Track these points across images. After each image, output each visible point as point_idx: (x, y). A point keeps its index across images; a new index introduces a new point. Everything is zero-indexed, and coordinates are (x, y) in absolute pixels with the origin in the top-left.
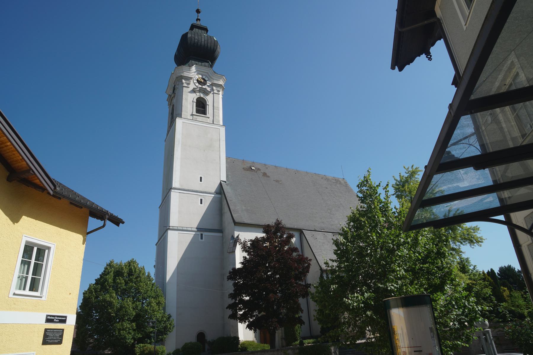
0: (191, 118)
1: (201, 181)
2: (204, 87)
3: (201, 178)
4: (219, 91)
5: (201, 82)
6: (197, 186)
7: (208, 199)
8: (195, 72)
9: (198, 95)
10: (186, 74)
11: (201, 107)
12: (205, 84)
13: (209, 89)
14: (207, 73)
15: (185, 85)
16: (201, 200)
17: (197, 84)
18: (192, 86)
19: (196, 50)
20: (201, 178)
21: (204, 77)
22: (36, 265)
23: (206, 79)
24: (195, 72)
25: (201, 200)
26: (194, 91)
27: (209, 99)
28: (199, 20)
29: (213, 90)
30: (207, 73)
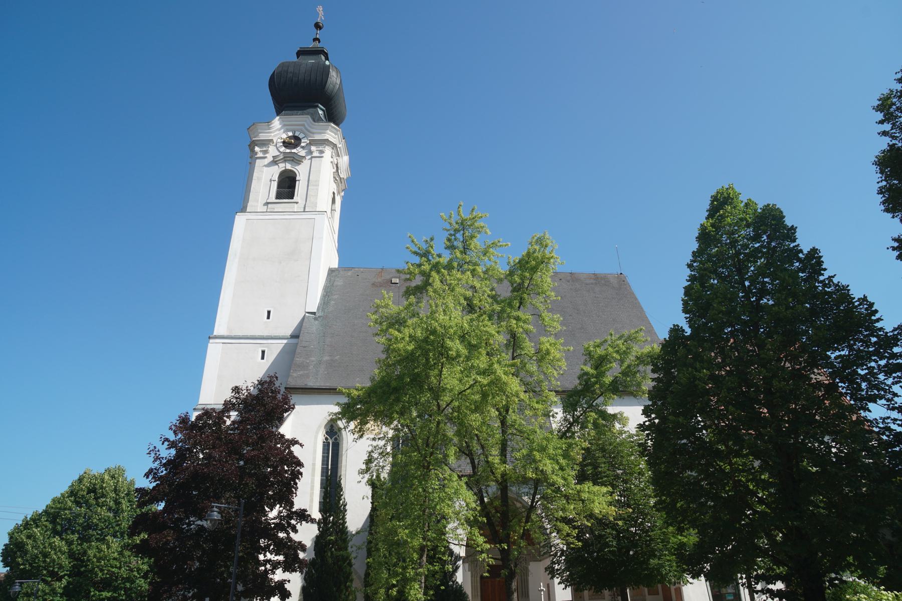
0: (264, 209)
1: (268, 318)
2: (294, 151)
3: (269, 312)
4: (322, 152)
5: (290, 144)
6: (261, 327)
7: (275, 349)
8: (280, 130)
9: (282, 166)
10: (263, 136)
11: (287, 186)
12: (295, 146)
13: (302, 153)
14: (303, 125)
15: (260, 155)
16: (263, 352)
17: (283, 149)
18: (272, 151)
19: (302, 92)
20: (269, 312)
21: (297, 134)
22: (328, 465)
23: (301, 136)
24: (280, 130)
25: (263, 352)
26: (275, 162)
27: (301, 171)
28: (318, 40)
29: (311, 152)
30: (303, 125)
